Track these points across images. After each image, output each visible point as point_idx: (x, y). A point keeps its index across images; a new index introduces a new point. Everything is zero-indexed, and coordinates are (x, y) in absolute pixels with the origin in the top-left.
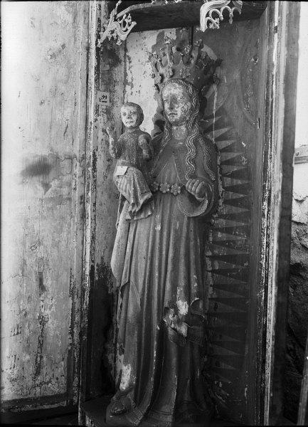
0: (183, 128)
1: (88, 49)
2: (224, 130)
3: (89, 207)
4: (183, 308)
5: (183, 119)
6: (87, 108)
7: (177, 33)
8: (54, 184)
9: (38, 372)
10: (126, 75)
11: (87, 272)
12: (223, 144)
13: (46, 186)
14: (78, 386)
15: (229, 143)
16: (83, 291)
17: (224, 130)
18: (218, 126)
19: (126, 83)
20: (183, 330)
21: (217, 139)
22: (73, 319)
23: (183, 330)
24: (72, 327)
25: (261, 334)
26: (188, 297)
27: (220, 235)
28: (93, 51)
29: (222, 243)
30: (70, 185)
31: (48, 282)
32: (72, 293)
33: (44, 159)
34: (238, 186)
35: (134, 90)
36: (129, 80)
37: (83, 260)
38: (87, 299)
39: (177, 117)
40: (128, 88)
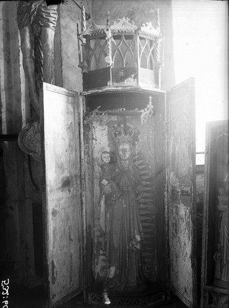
0: (127, 162)
1: (79, 124)
2: (141, 161)
3: (84, 199)
4: (138, 238)
5: (129, 159)
6: (80, 152)
7: (118, 118)
8: (72, 189)
9: (71, 281)
10: (93, 135)
11: (85, 229)
12: (141, 167)
13: (69, 191)
14: (84, 282)
15: (144, 166)
16: (83, 238)
17: (141, 161)
18: (138, 159)
19: (93, 139)
20: (138, 247)
21: (139, 165)
22: (80, 252)
23: (138, 247)
24: (80, 256)
25: (166, 244)
26: (140, 233)
27: (142, 206)
28: (82, 126)
29: (143, 209)
30: (76, 189)
31: (72, 237)
32: (79, 239)
33: (68, 178)
34: (148, 185)
35: (97, 142)
36: (95, 138)
37: (83, 224)
38: (85, 242)
39: (127, 158)
40: (94, 141)
